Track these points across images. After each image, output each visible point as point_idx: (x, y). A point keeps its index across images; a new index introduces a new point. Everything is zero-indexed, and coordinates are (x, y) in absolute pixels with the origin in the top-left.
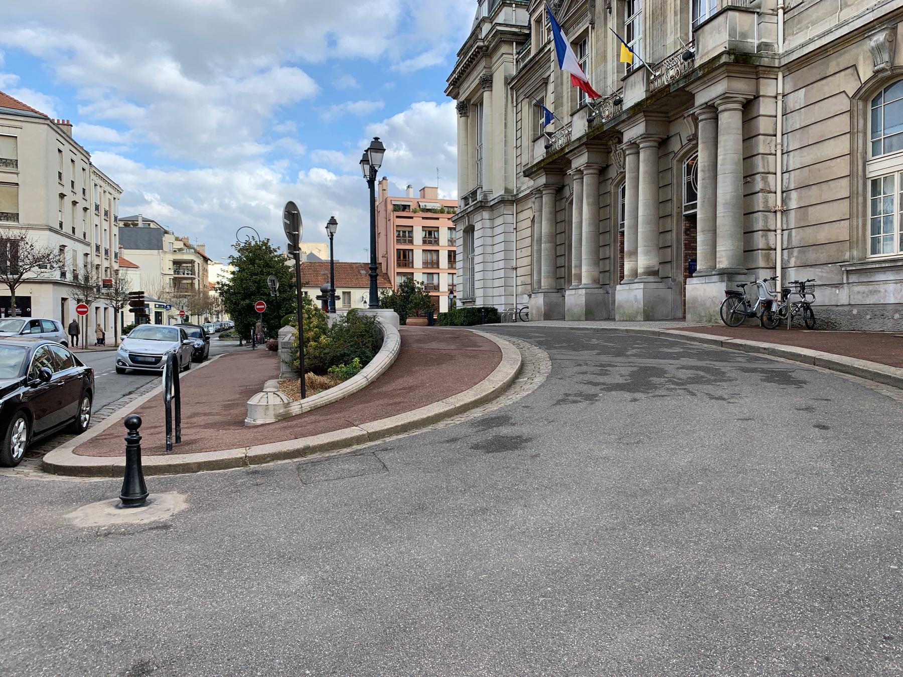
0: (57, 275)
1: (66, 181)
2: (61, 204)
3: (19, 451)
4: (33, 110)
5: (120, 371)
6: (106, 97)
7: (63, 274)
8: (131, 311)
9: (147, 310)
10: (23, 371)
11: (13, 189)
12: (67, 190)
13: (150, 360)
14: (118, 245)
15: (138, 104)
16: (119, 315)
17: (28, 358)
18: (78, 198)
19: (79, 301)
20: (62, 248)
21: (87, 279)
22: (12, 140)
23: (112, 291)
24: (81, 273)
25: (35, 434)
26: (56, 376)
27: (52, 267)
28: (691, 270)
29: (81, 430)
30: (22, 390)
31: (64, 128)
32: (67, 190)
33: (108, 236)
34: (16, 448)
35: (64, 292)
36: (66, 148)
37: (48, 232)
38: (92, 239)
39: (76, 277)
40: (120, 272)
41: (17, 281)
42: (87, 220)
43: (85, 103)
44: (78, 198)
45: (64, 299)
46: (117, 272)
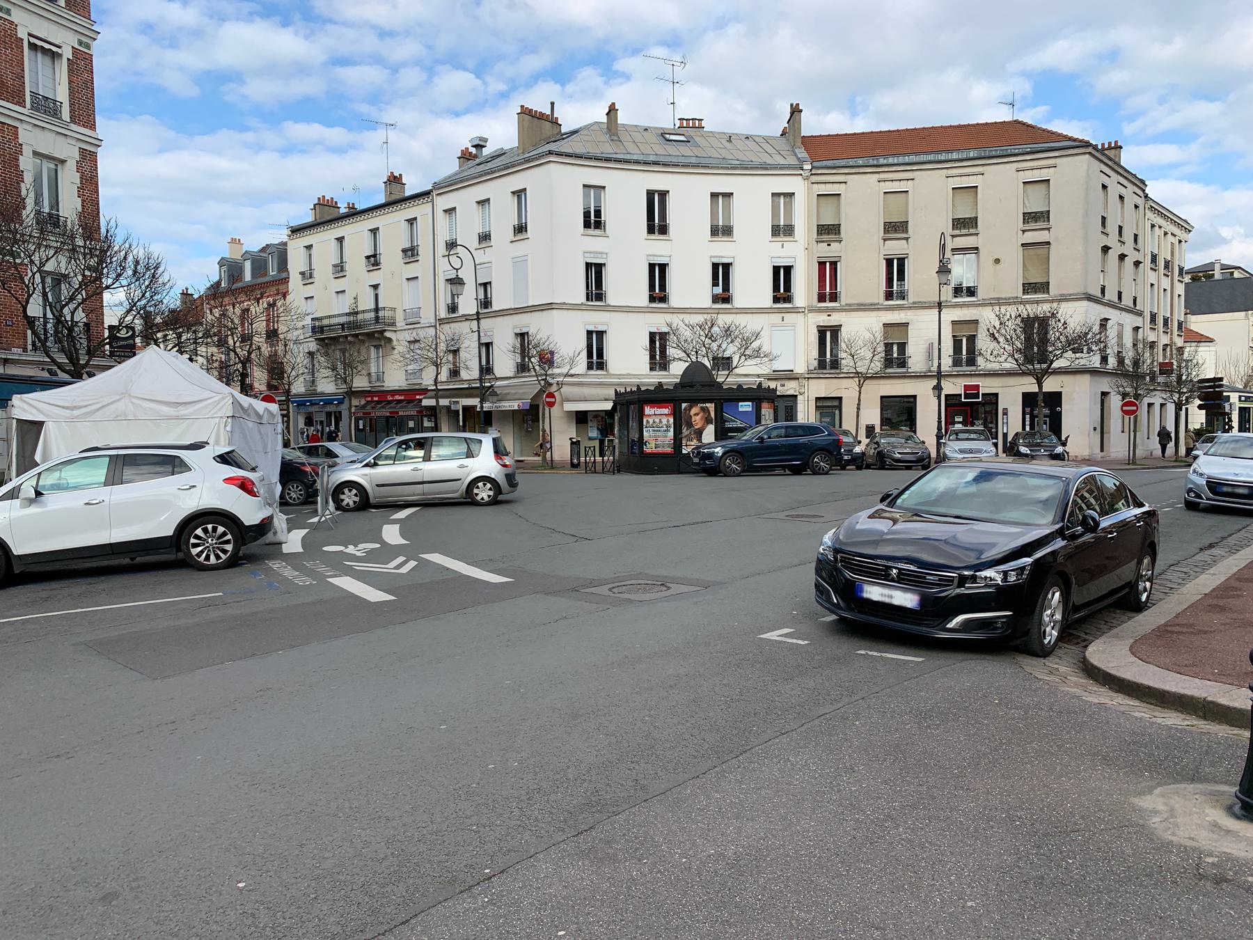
0: (1096, 361)
1: (1112, 228)
2: (1104, 261)
3: (1052, 634)
4: (1071, 139)
5: (1191, 506)
6: (1162, 100)
7: (1104, 359)
8: (1200, 407)
9: (1227, 406)
10: (1060, 514)
11: (1041, 251)
12: (1112, 241)
13: (1241, 491)
14: (1183, 310)
15: (1210, 98)
16: (1183, 413)
17: (1066, 492)
18: (1128, 249)
19: (1124, 395)
20: (1104, 322)
21: (1136, 363)
22: (1043, 187)
23: (1174, 378)
24: (1129, 356)
25: (1077, 609)
26: (1105, 523)
27: (1090, 350)
28: (86, 325)
29: (1139, 607)
30: (1059, 543)
31: (1111, 153)
32: (1112, 241)
33: (1166, 297)
34: (1048, 629)
35: (1105, 384)
36: (1113, 181)
37: (1085, 303)
38: (1146, 306)
39: (1121, 361)
40: (1187, 349)
41: (1046, 372)
42: (1138, 281)
43: (1132, 118)
44: (1128, 249)
45: (1104, 394)
46: (1181, 350)
